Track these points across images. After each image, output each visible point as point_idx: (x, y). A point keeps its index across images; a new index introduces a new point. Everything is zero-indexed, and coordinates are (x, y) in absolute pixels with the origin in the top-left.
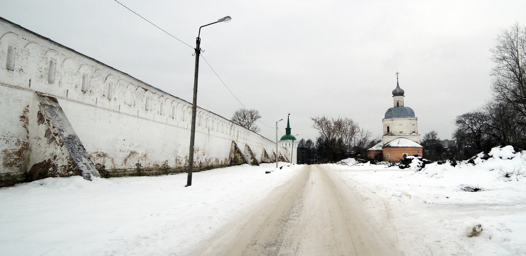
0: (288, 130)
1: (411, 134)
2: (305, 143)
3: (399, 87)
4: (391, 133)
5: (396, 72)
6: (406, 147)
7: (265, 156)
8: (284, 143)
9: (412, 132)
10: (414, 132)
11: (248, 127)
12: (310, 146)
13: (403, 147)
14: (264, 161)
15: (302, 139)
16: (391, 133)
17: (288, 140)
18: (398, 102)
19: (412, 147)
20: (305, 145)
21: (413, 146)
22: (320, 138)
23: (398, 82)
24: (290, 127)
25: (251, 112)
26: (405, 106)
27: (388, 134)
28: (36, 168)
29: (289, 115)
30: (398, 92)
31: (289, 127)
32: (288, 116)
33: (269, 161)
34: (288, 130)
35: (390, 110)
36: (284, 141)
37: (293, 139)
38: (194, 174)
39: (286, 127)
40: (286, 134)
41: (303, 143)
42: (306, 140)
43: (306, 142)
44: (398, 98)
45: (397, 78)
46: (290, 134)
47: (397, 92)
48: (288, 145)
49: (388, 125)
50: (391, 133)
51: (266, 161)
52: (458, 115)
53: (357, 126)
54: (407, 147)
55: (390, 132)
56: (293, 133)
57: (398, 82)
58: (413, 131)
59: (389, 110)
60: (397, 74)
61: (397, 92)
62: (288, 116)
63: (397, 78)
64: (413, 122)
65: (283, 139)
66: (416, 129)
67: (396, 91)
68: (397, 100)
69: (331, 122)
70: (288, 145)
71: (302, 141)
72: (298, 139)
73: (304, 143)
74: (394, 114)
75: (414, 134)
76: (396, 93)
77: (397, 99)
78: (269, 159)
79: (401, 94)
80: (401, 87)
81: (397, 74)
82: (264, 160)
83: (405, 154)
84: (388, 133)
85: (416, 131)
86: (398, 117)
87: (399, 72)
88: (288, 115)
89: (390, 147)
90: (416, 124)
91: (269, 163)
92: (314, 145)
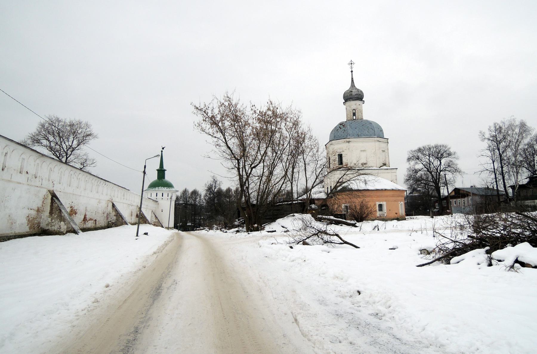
0: (161, 172)
1: (381, 168)
2: (189, 195)
3: (354, 86)
4: (345, 166)
5: (349, 61)
6: (382, 190)
7: (51, 213)
8: (153, 193)
9: (382, 165)
10: (385, 164)
11: (67, 154)
12: (196, 199)
13: (378, 190)
14: (47, 228)
15: (186, 190)
16: (346, 165)
17: (160, 187)
18: (354, 111)
19: (393, 190)
20: (189, 197)
21: (394, 188)
22: (211, 186)
23: (352, 79)
24: (165, 168)
25: (71, 125)
26: (364, 119)
27: (340, 168)
28: (228, 219)
29: (163, 148)
30: (355, 93)
31: (163, 168)
32: (162, 151)
33: (63, 227)
34: (161, 172)
35: (342, 125)
36: (154, 189)
37: (169, 185)
38: (168, 227)
39: (158, 168)
40: (157, 179)
41: (186, 194)
42: (190, 190)
43: (190, 193)
44: (353, 104)
45: (352, 72)
46: (164, 178)
47: (353, 93)
48: (160, 195)
49: (341, 151)
50: (346, 165)
51: (55, 228)
52: (409, 149)
53: (308, 136)
54: (385, 190)
55: (344, 164)
56: (168, 177)
57: (352, 79)
58: (383, 162)
59: (341, 124)
60: (351, 64)
61: (353, 93)
62: (162, 151)
63: (352, 72)
64: (383, 145)
65: (153, 185)
66: (387, 160)
67: (352, 91)
68: (353, 109)
69: (248, 112)
70: (160, 195)
71: (185, 192)
72: (179, 189)
73: (187, 195)
74: (350, 131)
75: (385, 167)
76: (351, 95)
77: (354, 107)
78: (62, 223)
79: (359, 97)
80: (358, 85)
81: (351, 64)
82: (47, 225)
83: (381, 203)
84: (340, 166)
85: (387, 163)
86: (358, 136)
87: (353, 61)
88: (161, 149)
89: (351, 190)
90: (386, 151)
91: (64, 234)
92: (202, 197)
